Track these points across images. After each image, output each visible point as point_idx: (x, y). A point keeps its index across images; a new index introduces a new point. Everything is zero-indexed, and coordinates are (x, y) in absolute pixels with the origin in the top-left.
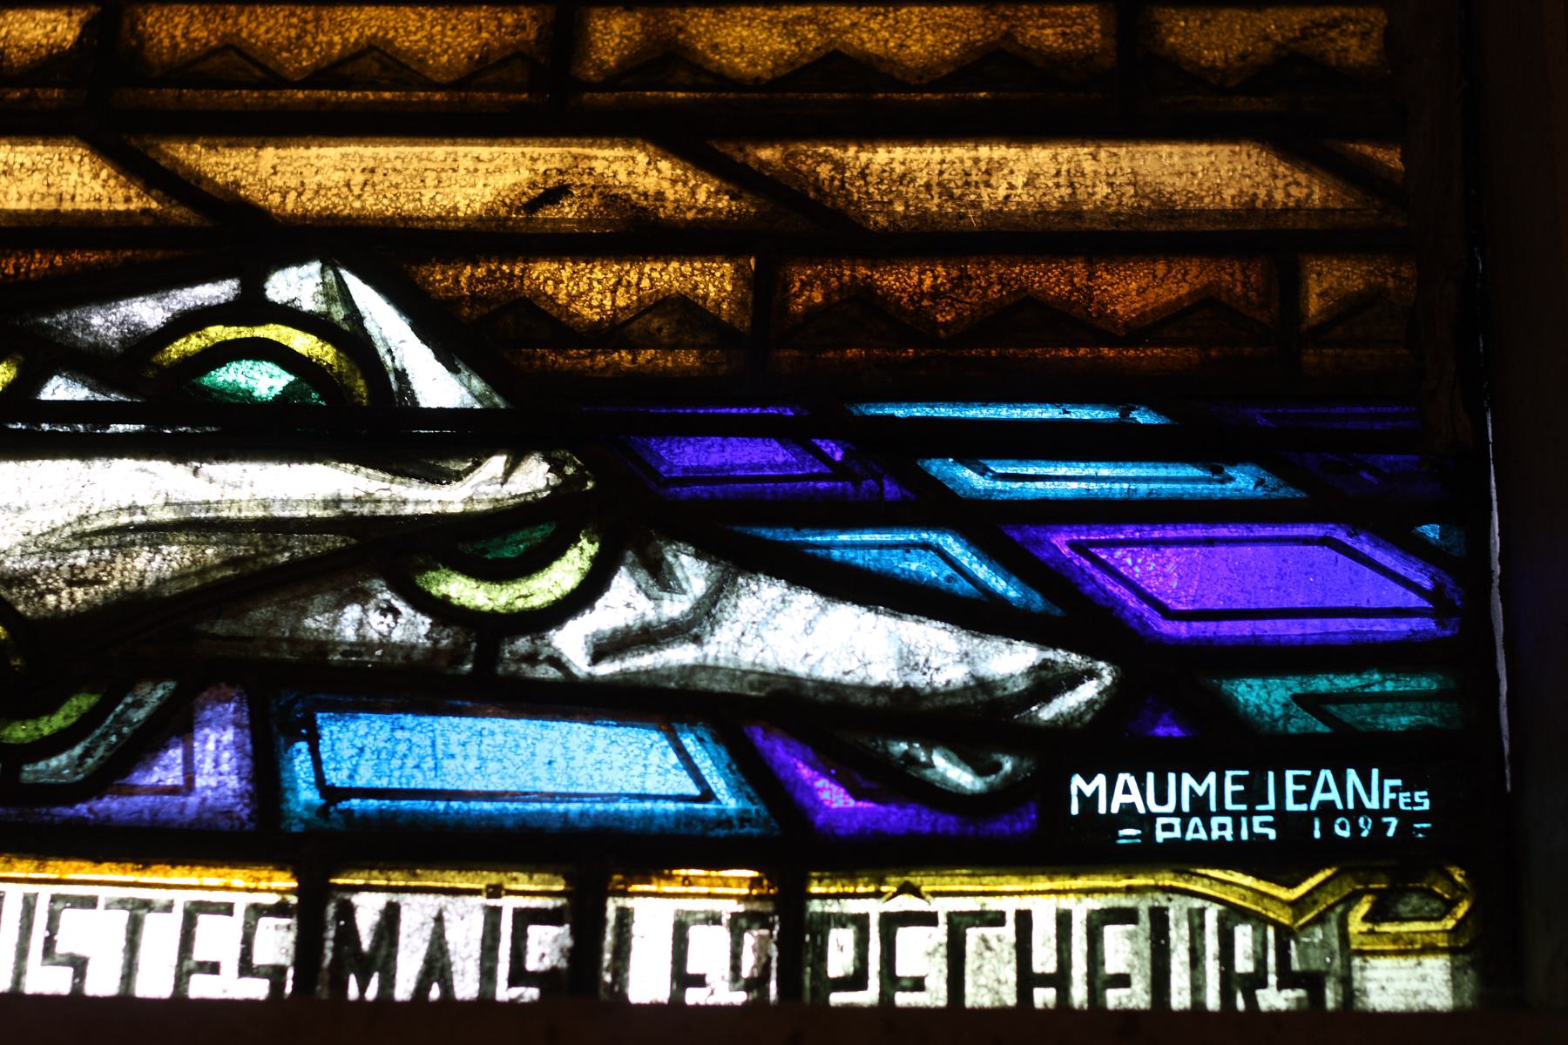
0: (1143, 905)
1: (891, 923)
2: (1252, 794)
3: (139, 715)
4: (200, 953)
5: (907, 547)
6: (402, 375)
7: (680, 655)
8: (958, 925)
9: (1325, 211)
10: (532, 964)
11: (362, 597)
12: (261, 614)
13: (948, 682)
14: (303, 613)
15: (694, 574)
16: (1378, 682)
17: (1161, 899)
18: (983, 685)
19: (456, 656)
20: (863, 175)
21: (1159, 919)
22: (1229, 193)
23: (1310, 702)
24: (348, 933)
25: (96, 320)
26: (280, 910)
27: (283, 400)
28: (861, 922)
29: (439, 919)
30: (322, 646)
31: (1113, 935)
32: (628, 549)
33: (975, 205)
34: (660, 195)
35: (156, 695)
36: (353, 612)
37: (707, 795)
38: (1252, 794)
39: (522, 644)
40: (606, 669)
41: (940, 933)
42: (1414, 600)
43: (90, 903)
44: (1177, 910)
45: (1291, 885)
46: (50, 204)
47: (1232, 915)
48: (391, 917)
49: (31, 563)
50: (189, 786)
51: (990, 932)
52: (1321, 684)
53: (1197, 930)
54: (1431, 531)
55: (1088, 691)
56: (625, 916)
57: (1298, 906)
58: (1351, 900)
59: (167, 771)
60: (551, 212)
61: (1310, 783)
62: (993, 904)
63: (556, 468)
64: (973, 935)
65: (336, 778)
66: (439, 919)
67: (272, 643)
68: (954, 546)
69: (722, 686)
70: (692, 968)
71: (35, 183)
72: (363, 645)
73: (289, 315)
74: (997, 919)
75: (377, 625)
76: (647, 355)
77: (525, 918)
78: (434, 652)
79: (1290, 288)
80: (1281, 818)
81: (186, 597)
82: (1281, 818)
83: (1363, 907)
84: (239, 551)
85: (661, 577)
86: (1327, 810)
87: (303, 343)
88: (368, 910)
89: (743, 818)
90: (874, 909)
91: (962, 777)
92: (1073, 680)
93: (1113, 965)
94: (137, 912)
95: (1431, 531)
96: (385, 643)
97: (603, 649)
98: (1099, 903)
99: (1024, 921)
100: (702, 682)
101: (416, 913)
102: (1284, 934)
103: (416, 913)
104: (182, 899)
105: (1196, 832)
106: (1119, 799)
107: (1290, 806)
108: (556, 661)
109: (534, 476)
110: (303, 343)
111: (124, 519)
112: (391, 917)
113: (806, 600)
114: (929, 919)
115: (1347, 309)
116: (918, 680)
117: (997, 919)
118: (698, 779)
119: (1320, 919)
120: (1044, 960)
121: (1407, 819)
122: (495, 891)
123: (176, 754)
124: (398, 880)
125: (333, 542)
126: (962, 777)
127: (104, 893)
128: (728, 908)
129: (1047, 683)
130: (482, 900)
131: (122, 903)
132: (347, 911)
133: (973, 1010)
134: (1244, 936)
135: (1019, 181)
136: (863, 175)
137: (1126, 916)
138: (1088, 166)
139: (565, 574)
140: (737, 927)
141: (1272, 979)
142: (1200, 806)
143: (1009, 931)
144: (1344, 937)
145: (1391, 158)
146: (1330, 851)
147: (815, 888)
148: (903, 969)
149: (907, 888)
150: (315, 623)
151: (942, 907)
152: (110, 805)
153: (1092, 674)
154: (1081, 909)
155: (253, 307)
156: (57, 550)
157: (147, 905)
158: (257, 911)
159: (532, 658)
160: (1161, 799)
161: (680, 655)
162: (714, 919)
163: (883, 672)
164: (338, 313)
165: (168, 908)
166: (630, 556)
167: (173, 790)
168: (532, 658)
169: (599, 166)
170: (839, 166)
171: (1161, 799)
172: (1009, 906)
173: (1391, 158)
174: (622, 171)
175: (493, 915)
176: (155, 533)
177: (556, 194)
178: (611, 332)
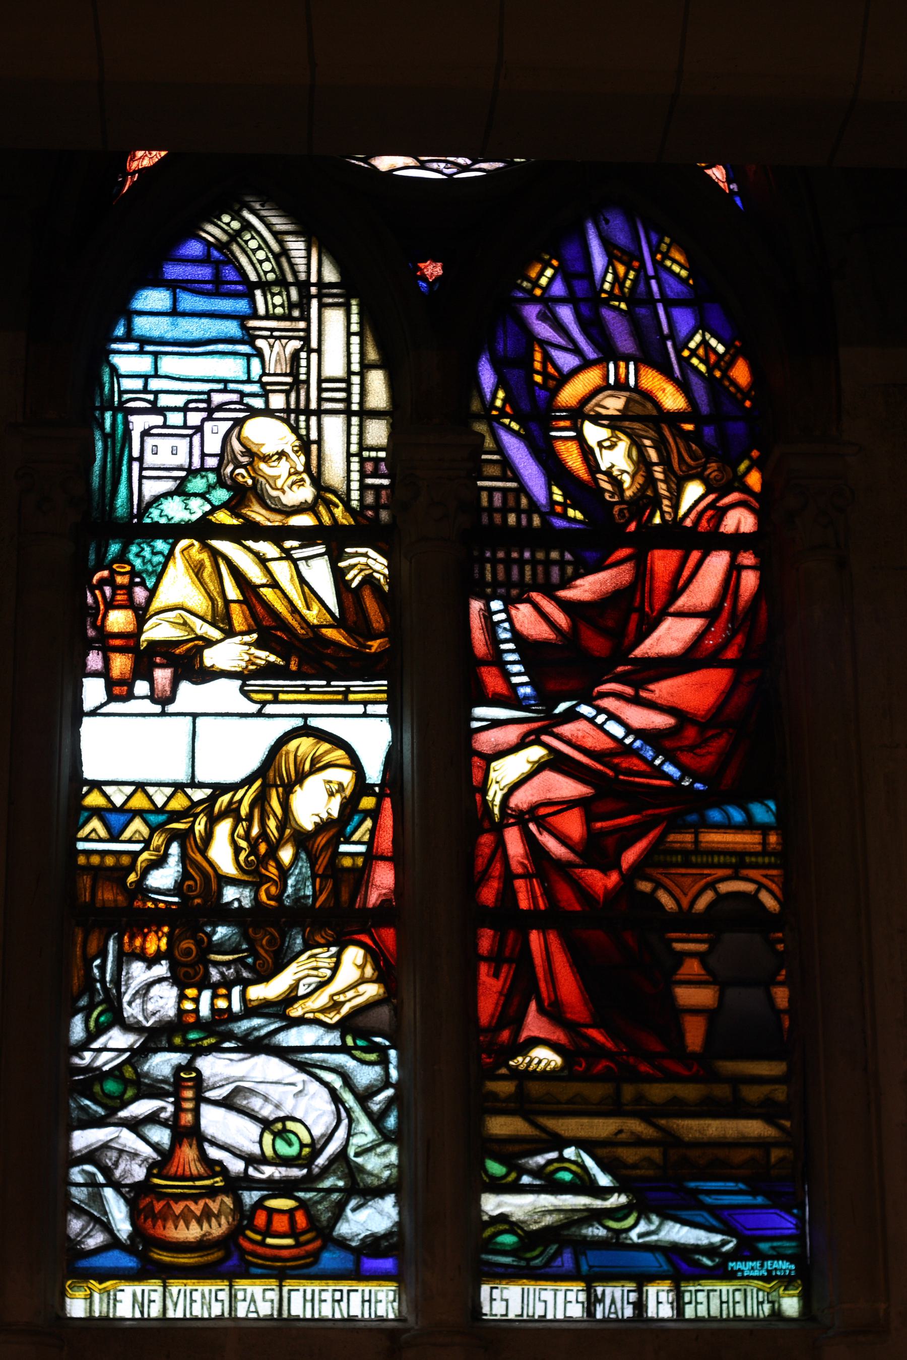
0: (743, 1288)
1: (697, 1291)
2: (762, 1266)
3: (552, 1251)
4: (568, 1299)
5: (697, 1215)
6: (594, 1175)
7: (654, 1238)
8: (709, 1291)
9: (775, 1137)
10: (631, 1300)
11: (592, 1226)
12: (573, 1229)
13: (213, 666)
14: (581, 1229)
15: (655, 1219)
16: (787, 1244)
17: (745, 1287)
18: (711, 1244)
19: (612, 1238)
20: (683, 1127)
21: (745, 1290)
22: (756, 1132)
23: (773, 1248)
24: (596, 1295)
25: (530, 1162)
26: (582, 1290)
27: (571, 1182)
28: (690, 1291)
29: (613, 1292)
30: (585, 1237)
31: (737, 1293)
32: (96, 634)
33: (706, 1135)
34: (642, 1132)
35: (554, 1247)
36: (590, 1229)
37: (661, 1266)
38: (762, 1266)
39: (624, 1235)
40: (641, 1241)
41: (705, 1294)
42: (792, 1226)
43: (546, 1289)
44: (749, 1289)
45: (769, 1283)
46: (515, 1133)
47: (759, 1290)
48: (604, 1291)
49: (526, 1218)
50: (563, 1265)
51: (715, 1293)
52: (775, 1244)
53: (752, 1293)
54: (795, 1211)
55: (731, 1245)
56: (647, 1291)
57: (771, 1288)
58: (780, 1287)
59: (558, 1262)
60: (620, 1136)
61: (772, 1263)
62: (715, 1288)
63: (628, 1197)
64: (711, 1294)
65: (591, 1263)
66: (613, 1292)
67: (576, 1236)
68: (705, 1214)
69: (662, 1244)
70: (660, 1300)
71: (512, 1128)
72: (593, 1236)
73: (569, 1161)
74: (715, 1291)
75: (596, 1232)
76: (643, 1171)
77: (629, 1291)
78: (607, 1237)
79: (768, 1155)
80: (768, 1271)
81: (558, 1226)
82: (768, 1271)
83: (782, 1288)
84: (568, 1216)
85: (650, 1221)
86: (776, 1269)
87: (574, 1168)
88: (599, 1290)
89: (668, 1271)
90: (693, 1289)
91: (708, 1263)
92: (728, 1242)
93: (737, 1299)
94: (556, 1291)
95: (795, 1211)
96: (598, 1236)
97: (640, 1236)
98: (734, 1288)
99: (721, 1291)
100: (659, 1243)
101: (608, 1291)
102: (768, 1294)
103: (608, 1291)
104: (564, 1288)
105: (752, 1274)
106: (738, 1267)
107: (769, 1268)
108: (631, 1239)
109: (623, 1199)
110: (574, 1168)
111: (543, 1209)
112: (604, 1291)
113: (678, 1226)
114: (703, 1291)
115: (782, 1160)
116: (699, 1243)
117: (715, 1291)
118: (659, 1263)
119: (775, 1291)
120: (724, 1299)
121: (791, 1271)
122: (623, 1286)
123: (559, 1259)
124: (605, 1284)
125: (585, 1214)
126: (708, 1263)
127: (549, 1288)
128: (666, 1288)
129: (724, 1243)
130: (620, 1288)
131: (552, 1290)
132: (595, 1291)
133: (82, 682)
134: (761, 1294)
135: (714, 1129)
136: (683, 1127)
137: (739, 1290)
138: (728, 1126)
139: (630, 1221)
140: (668, 1291)
141: (766, 1302)
142: (753, 1268)
143: (718, 1293)
144: (779, 1294)
145: (787, 1124)
146: (777, 1277)
147: (682, 1285)
148: (699, 1300)
149: (699, 1285)
150: (584, 1231)
151: (706, 1288)
152: (548, 1270)
153: (731, 1241)
154: (731, 1289)
155: (561, 1159)
156: (531, 1215)
157: (557, 1290)
158: (578, 1291)
159: (626, 1238)
160: (745, 1266)
161: (654, 1238)
162: (663, 1291)
163: (692, 1241)
164: (580, 1160)
165: (561, 1290)
166: (643, 1216)
167: (560, 1267)
168: (626, 1238)
169: (629, 1125)
170: (678, 1125)
171: (745, 1266)
172: (718, 1288)
173: (787, 1124)
174: (633, 1125)
175: (623, 1291)
176: (550, 1212)
177: (620, 1131)
178: (635, 1166)
